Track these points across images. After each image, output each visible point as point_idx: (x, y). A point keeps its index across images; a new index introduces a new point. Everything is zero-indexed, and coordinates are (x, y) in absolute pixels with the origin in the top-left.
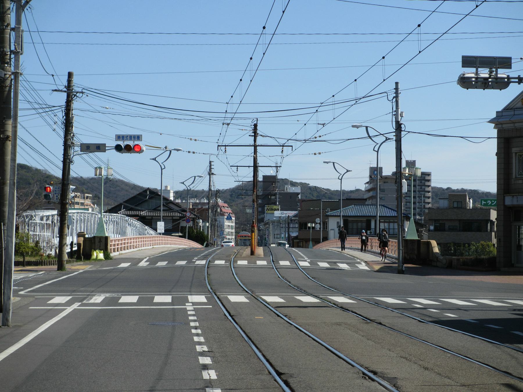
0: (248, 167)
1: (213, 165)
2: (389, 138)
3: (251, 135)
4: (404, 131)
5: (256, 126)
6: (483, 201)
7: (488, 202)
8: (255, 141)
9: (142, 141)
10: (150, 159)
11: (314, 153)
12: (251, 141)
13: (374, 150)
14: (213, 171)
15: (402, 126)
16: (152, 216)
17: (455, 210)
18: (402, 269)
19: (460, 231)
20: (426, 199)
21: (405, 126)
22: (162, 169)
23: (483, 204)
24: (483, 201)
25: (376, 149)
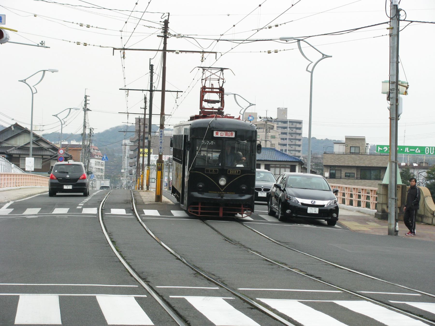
0: (142, 91)
1: (89, 100)
2: (326, 56)
3: (160, 35)
4: (404, 20)
5: (166, 23)
6: (379, 147)
7: (384, 149)
8: (165, 43)
9: (5, 15)
10: (19, 81)
11: (268, 51)
12: (158, 43)
13: (307, 70)
14: (88, 106)
15: (401, 13)
16: (20, 155)
17: (353, 156)
18: (395, 229)
19: (357, 179)
20: (296, 147)
21: (405, 13)
22: (33, 94)
23: (379, 150)
24: (379, 147)
25: (310, 69)
